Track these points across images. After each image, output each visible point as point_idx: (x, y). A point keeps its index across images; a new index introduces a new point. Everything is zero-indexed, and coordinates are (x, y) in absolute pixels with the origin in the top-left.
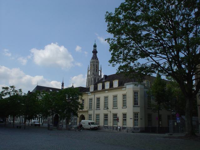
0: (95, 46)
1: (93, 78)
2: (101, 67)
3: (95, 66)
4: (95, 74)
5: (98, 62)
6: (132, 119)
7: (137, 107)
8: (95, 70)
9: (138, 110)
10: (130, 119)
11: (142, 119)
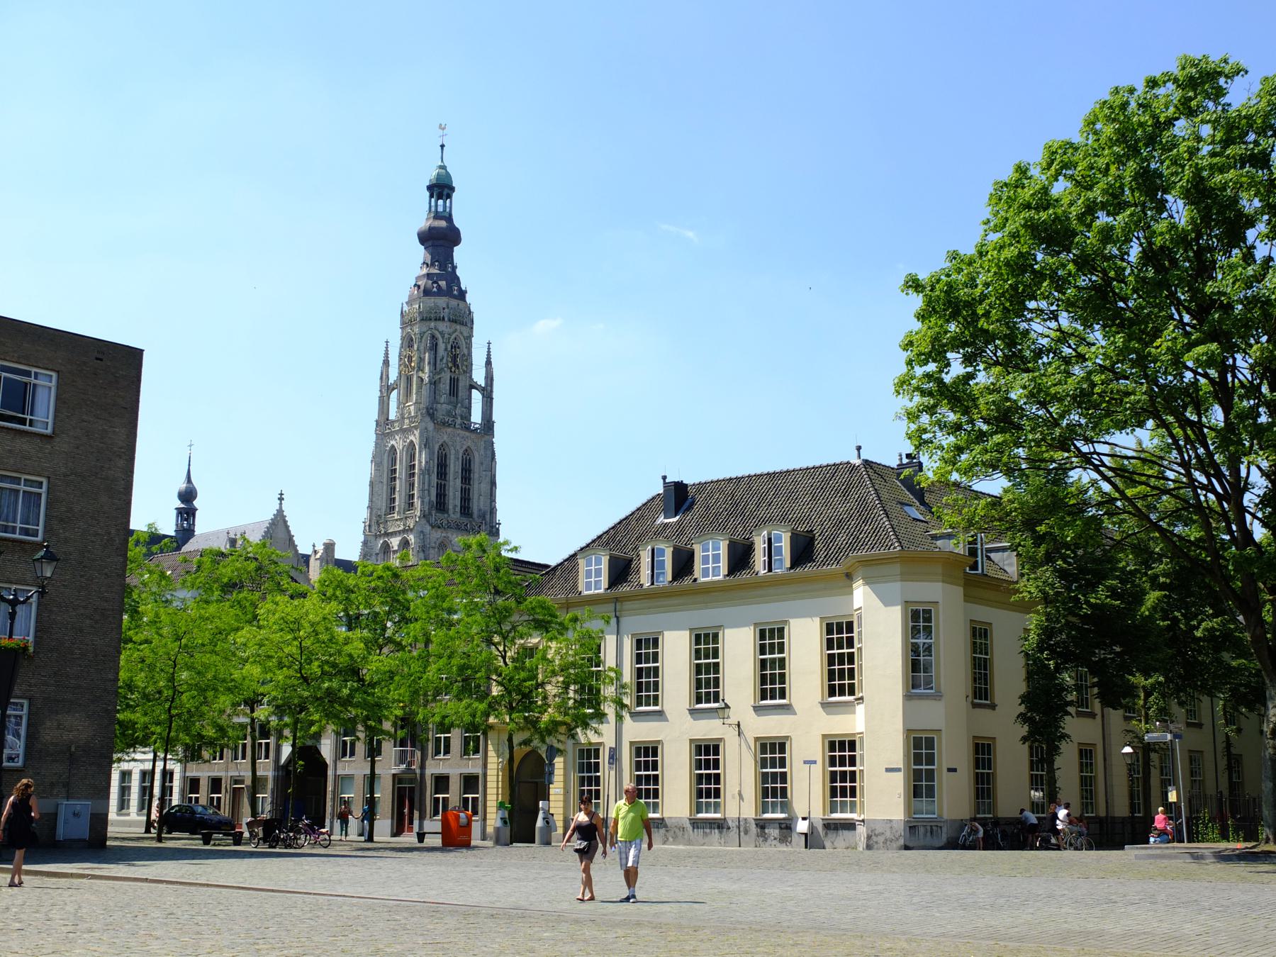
0: (441, 189)
1: (426, 444)
2: (489, 363)
3: (441, 346)
4: (440, 415)
5: (464, 319)
6: (898, 770)
7: (927, 697)
8: (445, 387)
9: (948, 716)
10: (888, 770)
11: (954, 770)
